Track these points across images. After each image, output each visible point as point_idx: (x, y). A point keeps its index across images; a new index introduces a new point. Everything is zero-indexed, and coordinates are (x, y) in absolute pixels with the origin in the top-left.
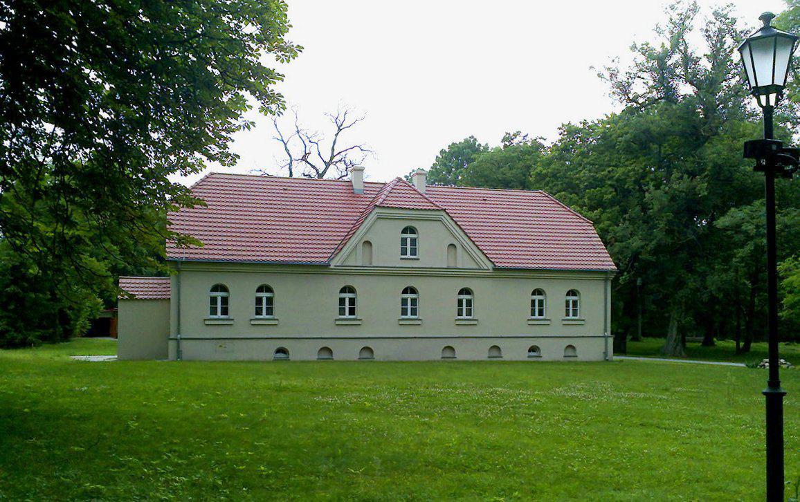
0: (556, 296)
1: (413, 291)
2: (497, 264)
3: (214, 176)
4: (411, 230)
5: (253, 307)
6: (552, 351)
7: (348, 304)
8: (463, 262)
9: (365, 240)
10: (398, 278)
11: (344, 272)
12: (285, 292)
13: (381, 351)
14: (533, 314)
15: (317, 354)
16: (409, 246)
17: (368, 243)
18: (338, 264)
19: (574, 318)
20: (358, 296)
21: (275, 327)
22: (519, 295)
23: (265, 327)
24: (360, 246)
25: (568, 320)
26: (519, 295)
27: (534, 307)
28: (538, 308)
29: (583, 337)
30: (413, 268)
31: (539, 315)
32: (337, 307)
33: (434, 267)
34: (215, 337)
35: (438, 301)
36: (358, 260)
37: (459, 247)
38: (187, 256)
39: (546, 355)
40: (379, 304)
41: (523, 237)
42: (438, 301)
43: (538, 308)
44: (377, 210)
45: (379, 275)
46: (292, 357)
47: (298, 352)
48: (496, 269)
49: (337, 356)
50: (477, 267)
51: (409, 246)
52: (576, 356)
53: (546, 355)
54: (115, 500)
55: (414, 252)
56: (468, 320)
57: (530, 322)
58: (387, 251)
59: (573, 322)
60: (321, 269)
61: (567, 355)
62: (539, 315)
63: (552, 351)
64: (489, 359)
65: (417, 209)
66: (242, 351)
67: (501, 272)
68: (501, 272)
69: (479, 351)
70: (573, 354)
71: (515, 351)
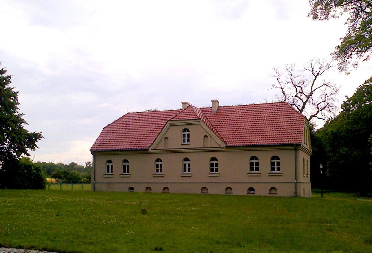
0: (264, 160)
1: (277, 158)
2: (228, 144)
3: (129, 114)
4: (186, 130)
5: (249, 166)
6: (262, 191)
7: (159, 168)
8: (210, 144)
9: (165, 136)
10: (170, 154)
11: (155, 152)
12: (134, 162)
13: (172, 189)
14: (157, 171)
15: (201, 190)
16: (186, 138)
17: (166, 138)
18: (153, 149)
19: (161, 173)
20: (249, 162)
21: (190, 177)
22: (242, 160)
23: (109, 178)
24: (163, 139)
25: (126, 175)
26: (242, 160)
27: (125, 168)
28: (254, 166)
29: (281, 183)
30: (183, 149)
31: (188, 172)
32: (259, 167)
33: (196, 147)
34: (250, 182)
35: (199, 164)
36: (161, 147)
37: (209, 137)
38: (296, 142)
39: (257, 192)
40: (172, 166)
41: (251, 127)
42: (199, 164)
43: (254, 166)
44: (169, 122)
45: (160, 153)
46: (135, 191)
47: (137, 188)
48: (227, 147)
49: (210, 192)
50: (219, 146)
51: (186, 138)
52: (232, 193)
53: (257, 192)
54: (244, 252)
55: (188, 141)
56: (216, 174)
57: (249, 175)
58: (175, 142)
59: (188, 175)
60: (145, 151)
61: (271, 193)
62: (188, 172)
63: (262, 191)
64: (225, 194)
65: (193, 119)
66: (116, 188)
67: (231, 148)
68: (231, 148)
69: (220, 190)
70: (275, 193)
71: (240, 191)
